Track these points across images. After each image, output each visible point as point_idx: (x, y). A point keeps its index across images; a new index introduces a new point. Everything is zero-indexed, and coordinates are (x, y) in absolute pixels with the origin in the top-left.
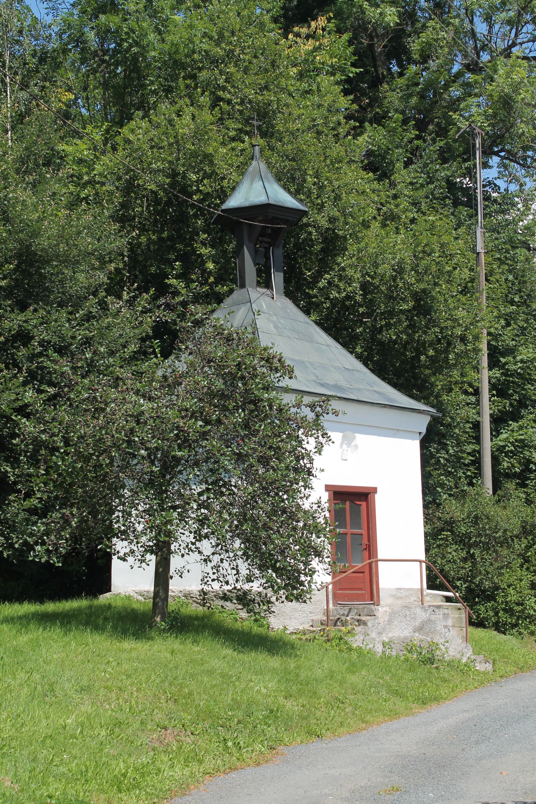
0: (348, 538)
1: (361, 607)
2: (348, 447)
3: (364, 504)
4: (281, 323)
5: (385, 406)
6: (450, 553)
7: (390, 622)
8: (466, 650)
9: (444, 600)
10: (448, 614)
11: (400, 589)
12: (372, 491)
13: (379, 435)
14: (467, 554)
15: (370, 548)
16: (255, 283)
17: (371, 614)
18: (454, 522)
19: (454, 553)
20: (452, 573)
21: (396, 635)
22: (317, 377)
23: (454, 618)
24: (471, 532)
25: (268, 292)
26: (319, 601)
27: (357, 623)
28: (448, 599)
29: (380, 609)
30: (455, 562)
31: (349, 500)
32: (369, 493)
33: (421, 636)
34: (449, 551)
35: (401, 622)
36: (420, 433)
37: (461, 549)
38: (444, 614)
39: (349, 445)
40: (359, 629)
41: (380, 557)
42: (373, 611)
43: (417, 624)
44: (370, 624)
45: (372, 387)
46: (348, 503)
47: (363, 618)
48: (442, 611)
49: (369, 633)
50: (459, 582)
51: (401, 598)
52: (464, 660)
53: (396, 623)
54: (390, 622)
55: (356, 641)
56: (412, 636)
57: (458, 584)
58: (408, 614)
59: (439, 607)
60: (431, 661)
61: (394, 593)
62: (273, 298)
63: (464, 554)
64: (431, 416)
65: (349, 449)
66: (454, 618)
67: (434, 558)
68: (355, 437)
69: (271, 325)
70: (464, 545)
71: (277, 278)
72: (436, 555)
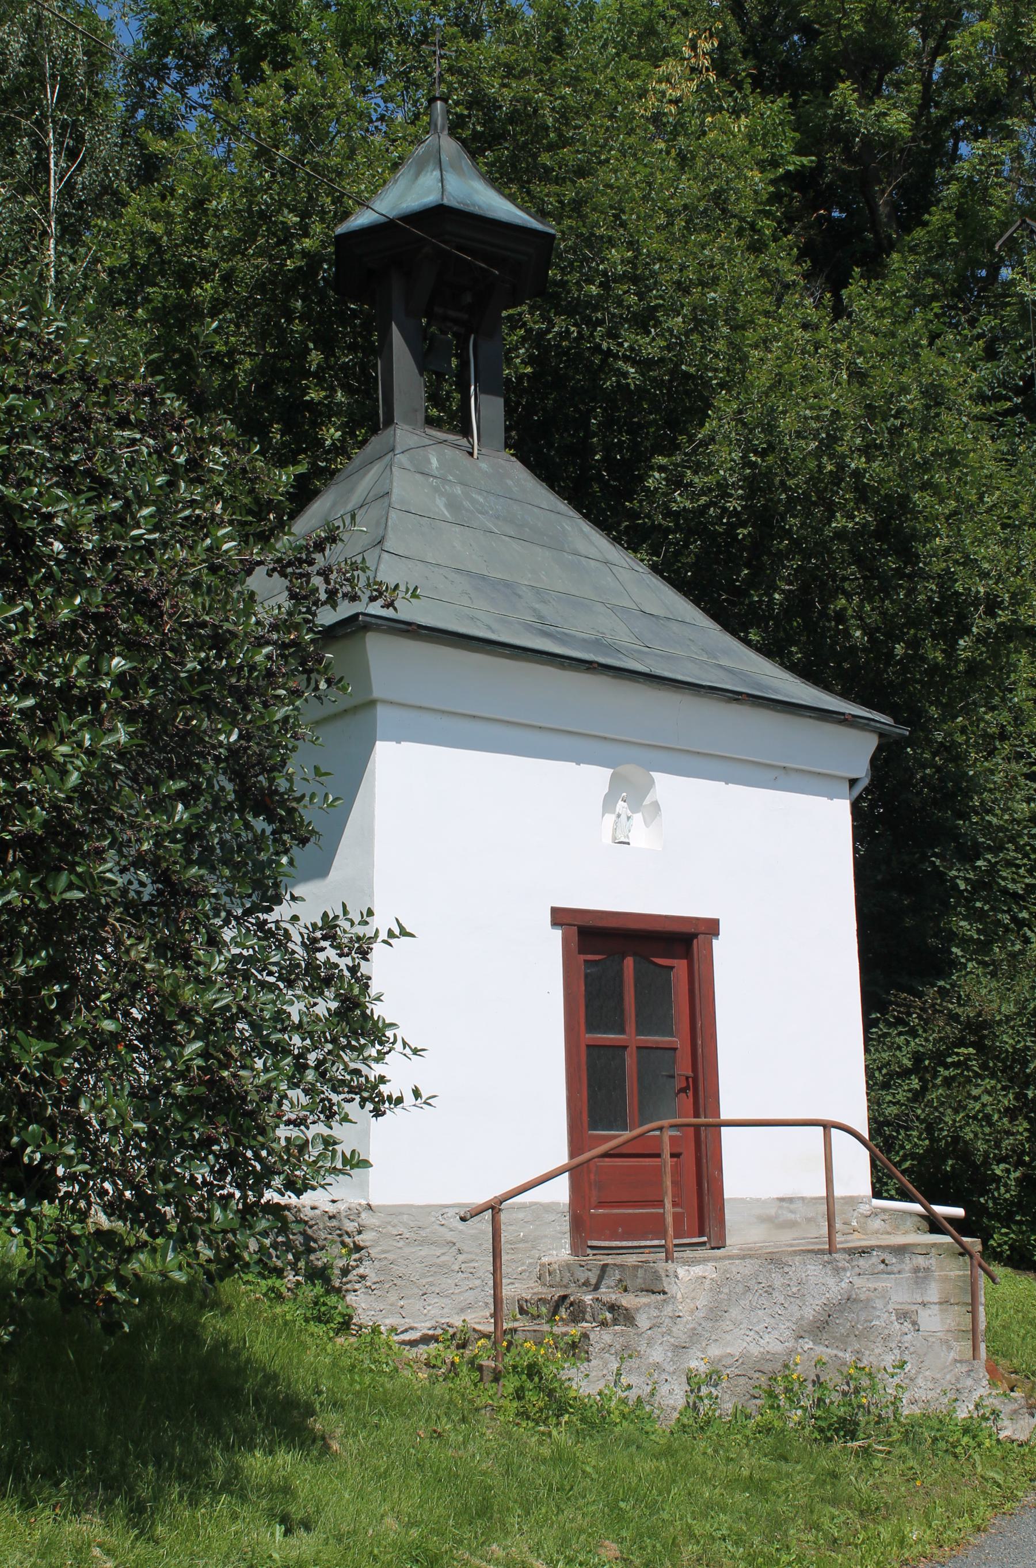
0: (630, 1061)
1: (631, 1259)
2: (634, 810)
3: (680, 966)
4: (473, 501)
5: (736, 697)
6: (977, 1099)
7: (716, 1313)
8: (969, 1382)
9: (925, 1225)
10: (927, 1270)
11: (791, 1200)
12: (703, 929)
13: (728, 779)
14: (1016, 1098)
15: (699, 1083)
16: (421, 417)
17: (654, 1288)
18: (985, 1025)
19: (986, 1098)
20: (981, 1146)
21: (735, 1350)
22: (540, 617)
23: (945, 1279)
24: (1028, 1048)
25: (464, 442)
26: (523, 1240)
27: (609, 1316)
28: (934, 1225)
29: (681, 1272)
30: (988, 1118)
31: (634, 954)
32: (695, 936)
33: (820, 1349)
34: (975, 1092)
35: (753, 1309)
36: (853, 782)
37: (1004, 1088)
38: (916, 1270)
39: (636, 805)
40: (601, 1338)
41: (725, 1115)
42: (658, 1278)
43: (809, 1313)
44: (643, 1321)
45: (715, 658)
46: (629, 962)
47: (627, 1301)
48: (909, 1263)
49: (642, 1348)
50: (1002, 1166)
51: (792, 1224)
52: (962, 1414)
53: (735, 1312)
54: (716, 1313)
55: (586, 1381)
56: (791, 1352)
57: (998, 1172)
58: (777, 1284)
59: (900, 1250)
60: (848, 1428)
61: (772, 1212)
62: (471, 454)
63: (1008, 1100)
64: (881, 735)
65: (638, 817)
66: (945, 1279)
67: (936, 1109)
68: (652, 782)
69: (440, 503)
70: (1011, 1080)
71: (487, 411)
72: (942, 1104)
